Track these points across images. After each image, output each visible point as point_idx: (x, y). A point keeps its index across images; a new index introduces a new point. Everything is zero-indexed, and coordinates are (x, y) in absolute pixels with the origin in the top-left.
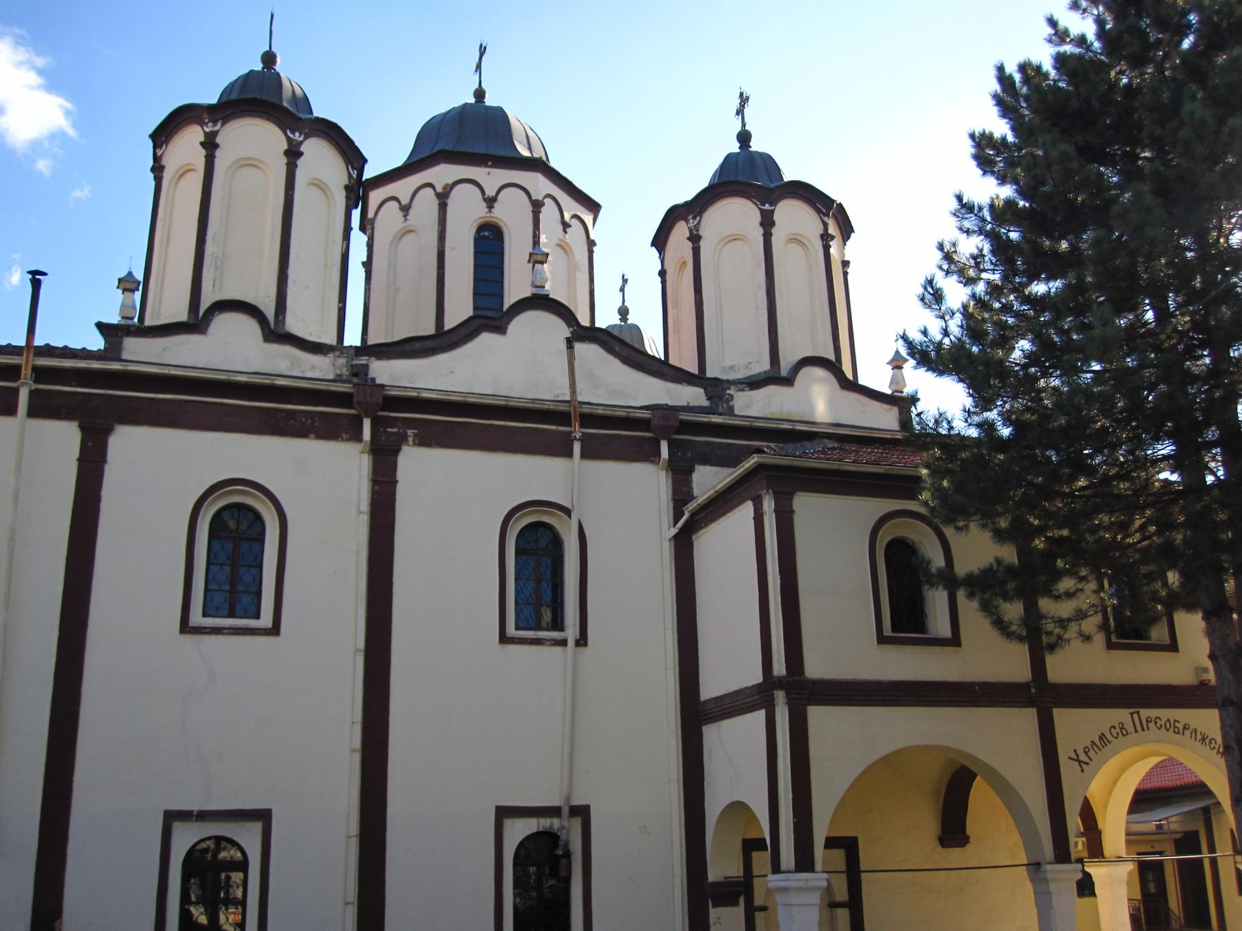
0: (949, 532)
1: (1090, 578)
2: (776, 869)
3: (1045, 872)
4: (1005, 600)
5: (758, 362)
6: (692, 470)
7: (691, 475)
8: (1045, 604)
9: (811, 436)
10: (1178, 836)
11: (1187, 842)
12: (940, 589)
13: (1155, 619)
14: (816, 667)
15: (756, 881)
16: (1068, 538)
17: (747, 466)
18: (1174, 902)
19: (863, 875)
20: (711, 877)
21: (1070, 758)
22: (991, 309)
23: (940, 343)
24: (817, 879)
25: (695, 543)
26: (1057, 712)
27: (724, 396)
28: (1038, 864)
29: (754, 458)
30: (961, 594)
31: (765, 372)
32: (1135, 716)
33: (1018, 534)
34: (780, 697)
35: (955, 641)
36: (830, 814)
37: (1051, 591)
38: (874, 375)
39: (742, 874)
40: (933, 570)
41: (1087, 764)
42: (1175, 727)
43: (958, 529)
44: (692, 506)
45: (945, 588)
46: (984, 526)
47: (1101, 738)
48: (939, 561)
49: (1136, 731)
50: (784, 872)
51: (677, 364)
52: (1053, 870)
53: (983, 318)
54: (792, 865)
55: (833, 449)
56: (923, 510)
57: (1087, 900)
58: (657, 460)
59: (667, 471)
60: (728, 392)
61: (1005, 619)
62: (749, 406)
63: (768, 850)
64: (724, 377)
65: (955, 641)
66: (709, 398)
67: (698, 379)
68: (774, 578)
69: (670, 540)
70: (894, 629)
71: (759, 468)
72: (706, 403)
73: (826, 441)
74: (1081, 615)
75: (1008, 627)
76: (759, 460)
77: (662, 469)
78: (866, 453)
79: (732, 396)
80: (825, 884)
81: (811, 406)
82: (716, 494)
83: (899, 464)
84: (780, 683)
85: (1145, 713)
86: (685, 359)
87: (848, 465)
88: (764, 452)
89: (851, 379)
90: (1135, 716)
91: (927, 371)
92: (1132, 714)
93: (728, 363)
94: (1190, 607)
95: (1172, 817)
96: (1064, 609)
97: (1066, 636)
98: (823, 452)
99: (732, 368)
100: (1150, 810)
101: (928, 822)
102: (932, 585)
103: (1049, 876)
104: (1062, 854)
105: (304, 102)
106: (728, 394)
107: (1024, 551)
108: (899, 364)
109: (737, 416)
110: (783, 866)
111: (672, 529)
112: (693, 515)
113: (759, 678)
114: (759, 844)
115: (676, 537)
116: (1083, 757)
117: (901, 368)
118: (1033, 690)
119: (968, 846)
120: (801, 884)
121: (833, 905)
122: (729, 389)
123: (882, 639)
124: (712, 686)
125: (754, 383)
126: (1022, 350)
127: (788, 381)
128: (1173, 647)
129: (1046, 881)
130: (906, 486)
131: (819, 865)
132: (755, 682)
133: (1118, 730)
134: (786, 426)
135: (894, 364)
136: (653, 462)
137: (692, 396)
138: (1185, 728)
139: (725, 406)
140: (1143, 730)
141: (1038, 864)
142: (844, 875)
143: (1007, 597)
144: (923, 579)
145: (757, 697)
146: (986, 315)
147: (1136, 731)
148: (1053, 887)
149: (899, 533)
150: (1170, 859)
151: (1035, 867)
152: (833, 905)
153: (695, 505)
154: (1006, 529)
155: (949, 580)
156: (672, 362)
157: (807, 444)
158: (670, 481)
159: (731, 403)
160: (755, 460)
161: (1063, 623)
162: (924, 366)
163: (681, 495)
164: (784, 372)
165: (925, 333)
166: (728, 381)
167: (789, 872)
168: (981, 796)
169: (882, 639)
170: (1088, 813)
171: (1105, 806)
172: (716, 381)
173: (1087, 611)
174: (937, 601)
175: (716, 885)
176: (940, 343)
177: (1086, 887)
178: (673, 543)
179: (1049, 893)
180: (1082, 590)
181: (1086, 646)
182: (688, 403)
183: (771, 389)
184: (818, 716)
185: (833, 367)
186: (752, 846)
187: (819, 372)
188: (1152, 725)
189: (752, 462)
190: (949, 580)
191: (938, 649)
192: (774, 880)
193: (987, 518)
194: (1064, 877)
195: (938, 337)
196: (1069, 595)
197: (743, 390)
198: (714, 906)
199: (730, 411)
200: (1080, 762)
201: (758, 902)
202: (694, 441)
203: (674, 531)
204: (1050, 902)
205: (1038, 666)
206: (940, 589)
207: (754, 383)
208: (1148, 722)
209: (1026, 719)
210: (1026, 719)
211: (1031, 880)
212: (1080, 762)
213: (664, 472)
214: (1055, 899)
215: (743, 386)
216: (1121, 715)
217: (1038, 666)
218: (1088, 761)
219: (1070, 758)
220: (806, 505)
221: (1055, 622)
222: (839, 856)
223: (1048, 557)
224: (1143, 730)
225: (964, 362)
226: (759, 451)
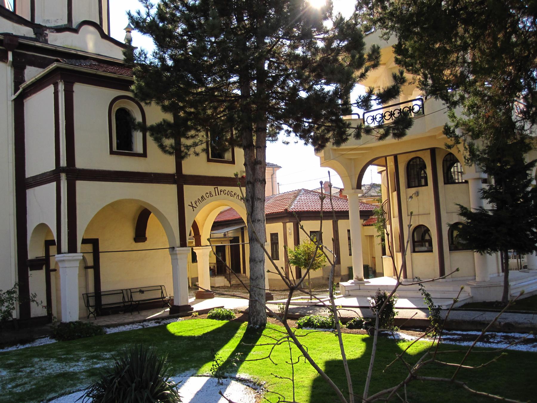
0: (143, 104)
1: (201, 130)
2: (59, 252)
3: (176, 251)
4: (166, 138)
5: (61, 19)
6: (25, 68)
7: (24, 70)
8: (183, 140)
9: (85, 58)
10: (231, 239)
11: (235, 240)
12: (139, 131)
13: (226, 150)
14: (80, 163)
15: (51, 258)
16: (193, 113)
17: (51, 67)
18: (228, 262)
19: (101, 254)
20: (30, 257)
21: (189, 205)
22: (170, 8)
23: (145, 19)
24: (78, 256)
25: (25, 104)
26: (185, 187)
27: (43, 34)
28: (173, 248)
29: (54, 64)
30: (148, 134)
31: (65, 25)
32: (216, 189)
33: (171, 108)
34: (63, 176)
35: (144, 155)
36: (85, 228)
37: (185, 135)
38: (119, 34)
39: (44, 255)
40: (136, 123)
41: (196, 208)
43: (146, 104)
44: (23, 85)
45: (141, 131)
46: (158, 103)
47: (202, 197)
48: (139, 119)
49: (216, 195)
50: (63, 253)
51: (20, 15)
52: (179, 250)
53: (167, 12)
54: (67, 250)
55: (95, 65)
56: (130, 95)
57: (195, 264)
58: (6, 61)
59: (11, 67)
60: (45, 32)
61: (164, 144)
62: (56, 40)
63: (55, 245)
64: (43, 24)
65: (144, 155)
66: (35, 34)
67: (31, 24)
68: (62, 121)
69: (12, 101)
70: (118, 148)
71: (57, 69)
72: (33, 36)
73: (92, 61)
74: (195, 145)
75: (165, 148)
76: (58, 65)
77: (9, 66)
78: (111, 68)
79: (47, 34)
80: (82, 258)
81: (86, 44)
82: (36, 80)
83: (125, 75)
84: (63, 170)
85: (220, 188)
86: (24, 13)
87: (100, 73)
88: (60, 62)
89: (107, 34)
90: (216, 189)
91: (139, 31)
92: (215, 188)
93: (46, 18)
94: (240, 146)
95: (230, 231)
96: (189, 142)
97: (189, 153)
98: (90, 66)
99: (48, 21)
100: (223, 229)
101: (130, 232)
102: (135, 129)
103: (177, 252)
104: (183, 244)
105: (129, 19)
106: (46, 33)
107: (176, 117)
108: (130, 30)
109: (49, 44)
110: (63, 251)
111: (13, 96)
112: (24, 90)
113: (54, 168)
114: (52, 242)
115: (15, 100)
116: (194, 205)
117: (130, 32)
118: (176, 177)
119: (146, 242)
120: (70, 258)
121: (87, 268)
122: (46, 31)
123: (112, 152)
124: (30, 172)
125: (59, 29)
126: (182, 28)
127: (76, 31)
128: (233, 162)
129: (176, 254)
130: (124, 84)
131: (79, 250)
132: (52, 169)
133: (209, 194)
134: (73, 52)
135: (127, 30)
136: (4, 62)
137: (26, 31)
138: (234, 194)
139: (43, 39)
140: (219, 195)
141: (173, 248)
142: (92, 254)
143: (167, 137)
144: (132, 127)
145: (52, 176)
146: (168, 10)
147: (216, 195)
148: (178, 256)
149: (123, 106)
150: (227, 244)
151: (172, 248)
152: (87, 268)
153: (25, 85)
154: (167, 106)
155: (143, 127)
156: (17, 13)
157: (82, 61)
158: (13, 72)
159: (47, 38)
160: (55, 65)
161: (188, 147)
162: (138, 29)
163: (18, 79)
164: (74, 26)
165: (139, 13)
166: (45, 27)
167: (65, 253)
168: (152, 221)
169: (112, 152)
170: (195, 226)
171: (203, 226)
172: (39, 26)
173: (198, 143)
174: (138, 137)
175: (32, 261)
176: (145, 19)
177: (194, 259)
178: (13, 102)
179: (177, 259)
180: (198, 135)
181: (196, 157)
182: (24, 35)
183: (67, 33)
184: (81, 185)
185: (99, 27)
186: (48, 243)
187: (91, 28)
189: (54, 66)
190: (143, 127)
191: (137, 158)
192: (58, 257)
193: (159, 101)
194: (185, 254)
195: (145, 16)
196: (192, 137)
197: (53, 32)
198: (31, 270)
199: (46, 42)
200: (193, 207)
201: (52, 267)
202: (26, 53)
203: (14, 97)
204: (178, 263)
205: (179, 166)
206: (139, 131)
207: (59, 29)
208: (221, 191)
209: (173, 189)
210: (173, 189)
211: (171, 254)
212: (193, 207)
213: (10, 67)
214: (179, 261)
215: (53, 30)
216: (210, 189)
217: (179, 166)
218: (196, 206)
219: (189, 205)
220: (79, 89)
221: (185, 147)
222: (89, 247)
223: (186, 120)
224: (219, 195)
225: (154, 28)
226: (57, 61)
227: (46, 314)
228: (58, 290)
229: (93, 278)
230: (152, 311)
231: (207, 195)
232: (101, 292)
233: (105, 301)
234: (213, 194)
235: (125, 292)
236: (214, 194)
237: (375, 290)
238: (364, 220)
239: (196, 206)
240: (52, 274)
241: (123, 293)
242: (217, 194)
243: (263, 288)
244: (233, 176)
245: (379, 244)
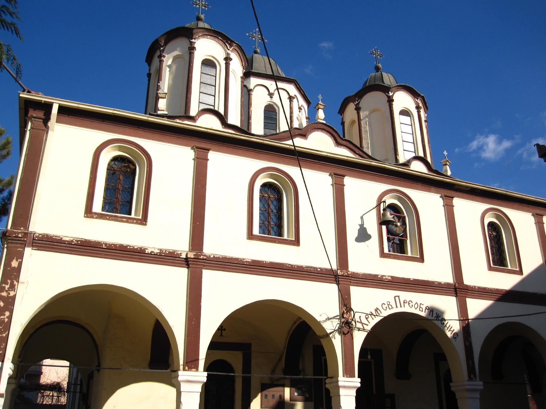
35: (296, 242)
41: (367, 325)
42: (420, 307)
49: (397, 307)
65: (296, 242)
140: (401, 307)
147: (397, 307)
188: (406, 305)
208: (404, 302)
224: (401, 307)
228: (239, 58)
231: (384, 306)
236: (394, 306)
237: (374, 208)
243: (461, 321)
244: (319, 321)
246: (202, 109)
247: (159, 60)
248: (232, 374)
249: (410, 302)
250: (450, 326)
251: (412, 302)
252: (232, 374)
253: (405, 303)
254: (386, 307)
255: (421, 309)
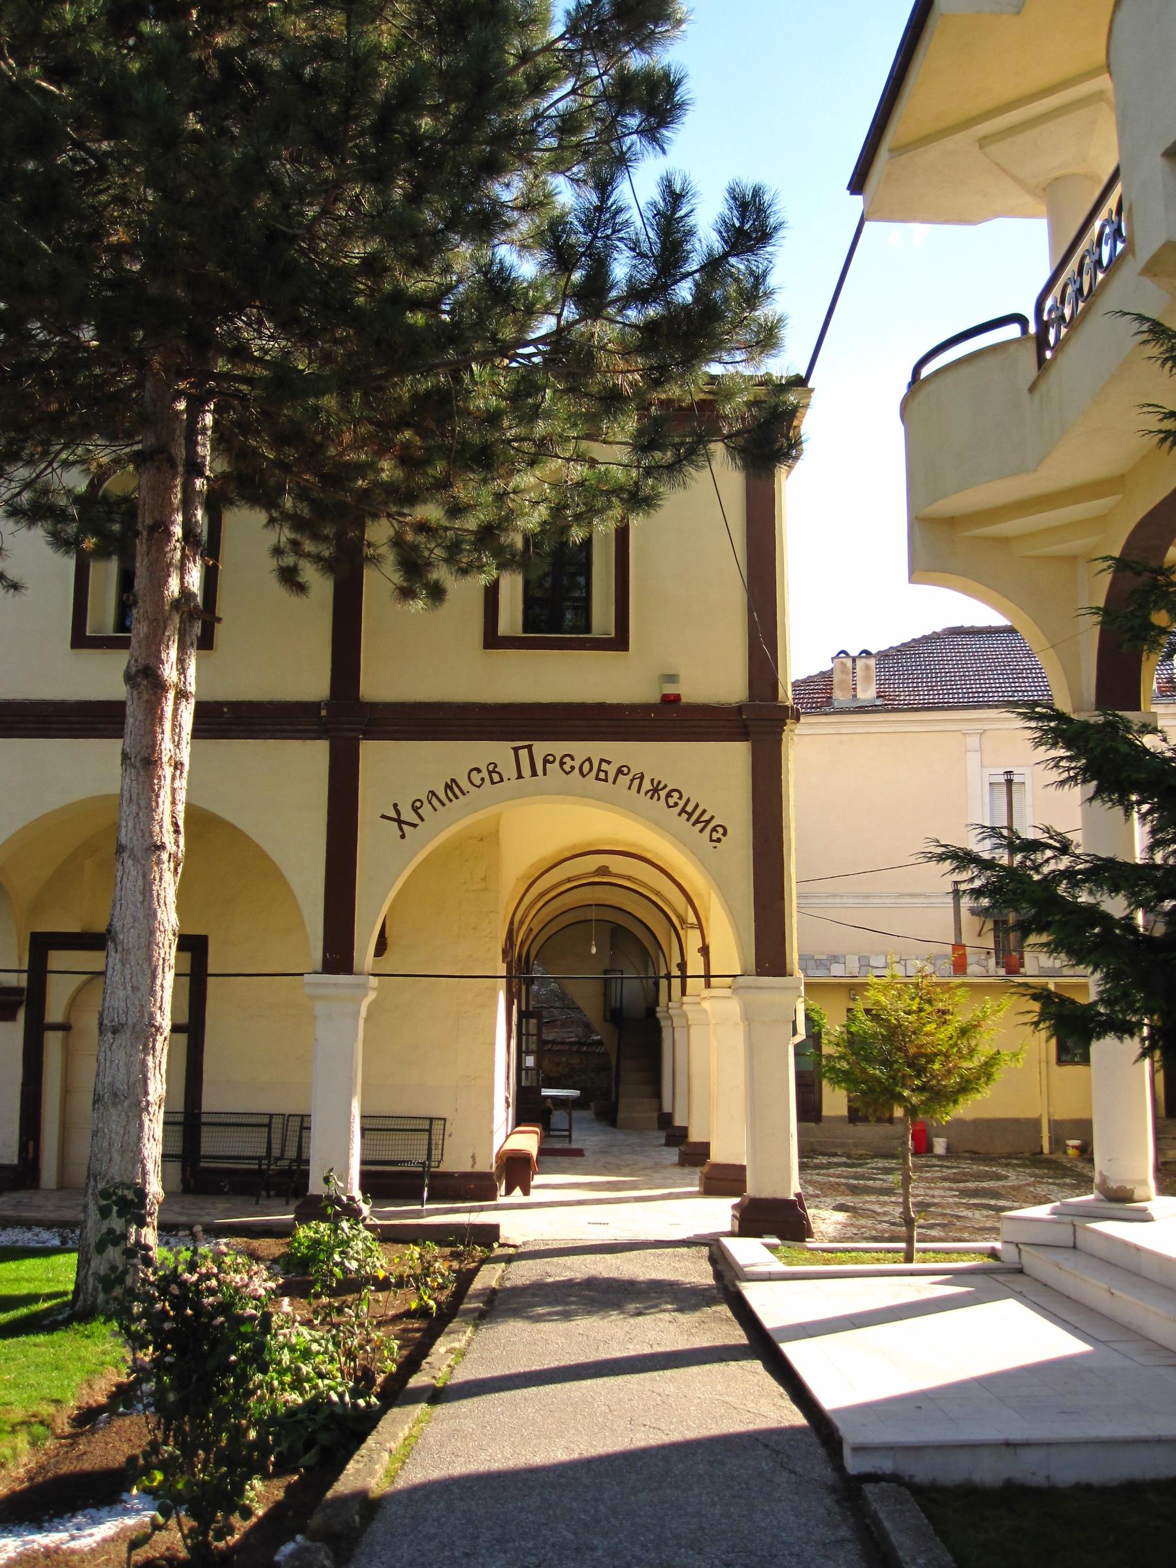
21: (383, 817)
32: (524, 753)
41: (415, 826)
42: (599, 770)
47: (447, 786)
49: (520, 776)
85: (541, 748)
90: (524, 753)
92: (516, 750)
116: (408, 815)
133: (485, 774)
140: (534, 774)
147: (520, 776)
152: (65, 1027)
200: (400, 822)
208: (546, 761)
212: (400, 822)
218: (416, 820)
219: (383, 817)
224: (534, 774)
227: (15, 1161)
229: (496, 1059)
230: (402, 1202)
232: (200, 1113)
233: (212, 1143)
234: (508, 769)
235: (277, 1123)
238: (405, 580)
239: (414, 819)
240: (53, 1042)
241: (269, 1126)
242: (526, 770)
245: (834, 1090)
246: (102, 1526)
247: (718, 1155)
248: (425, 1195)
249: (719, 829)
250: (697, 806)
251: (573, 759)
252: (425, 1195)
253: (548, 765)
254: (483, 779)
255: (602, 776)
